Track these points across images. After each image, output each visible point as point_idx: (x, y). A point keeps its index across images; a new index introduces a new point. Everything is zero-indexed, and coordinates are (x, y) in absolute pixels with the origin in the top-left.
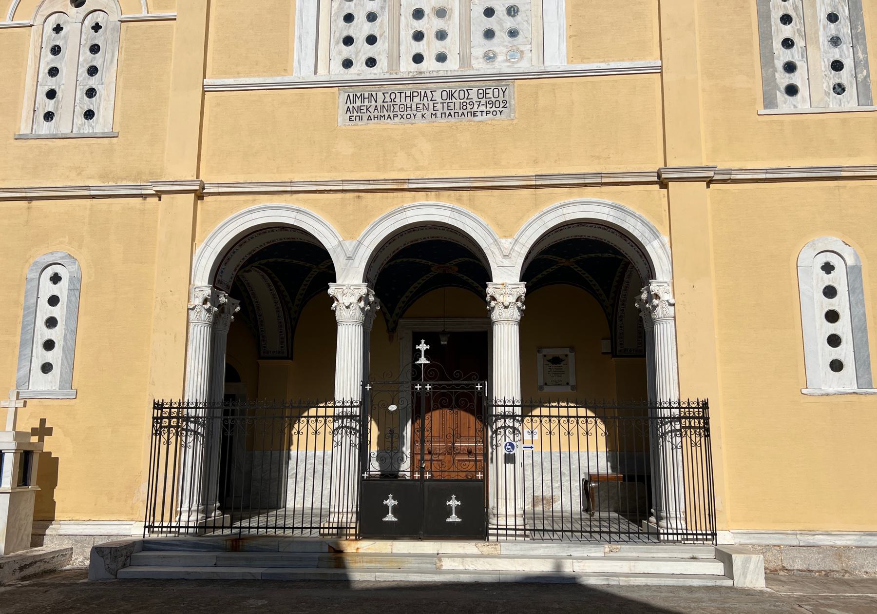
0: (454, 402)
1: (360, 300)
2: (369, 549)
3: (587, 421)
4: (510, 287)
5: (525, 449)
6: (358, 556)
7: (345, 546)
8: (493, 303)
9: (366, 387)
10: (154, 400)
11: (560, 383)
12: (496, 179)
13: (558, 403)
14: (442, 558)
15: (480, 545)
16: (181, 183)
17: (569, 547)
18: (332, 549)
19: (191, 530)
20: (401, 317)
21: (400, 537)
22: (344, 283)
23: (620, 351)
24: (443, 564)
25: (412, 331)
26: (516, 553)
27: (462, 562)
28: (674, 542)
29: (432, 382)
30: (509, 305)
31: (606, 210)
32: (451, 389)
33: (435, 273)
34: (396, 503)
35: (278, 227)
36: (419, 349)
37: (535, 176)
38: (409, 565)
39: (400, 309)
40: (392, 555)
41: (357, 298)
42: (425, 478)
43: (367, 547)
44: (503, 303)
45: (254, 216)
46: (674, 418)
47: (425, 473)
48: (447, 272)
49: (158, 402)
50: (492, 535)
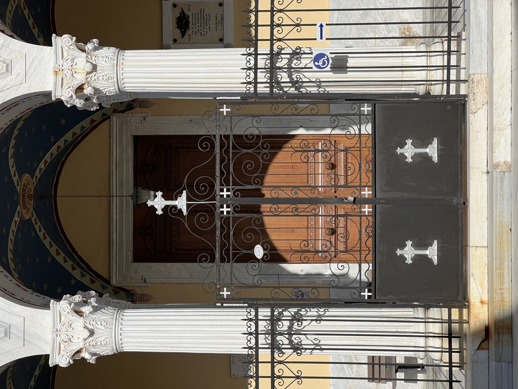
0: (250, 151)
1: (79, 313)
2: (481, 284)
3: (279, 25)
4: (60, 62)
5: (324, 37)
6: (493, 302)
7: (478, 324)
8: (88, 91)
9: (225, 297)
11: (219, 18)
13: (251, 11)
14: (494, 161)
15: (474, 107)
18: (483, 344)
20: (108, 282)
21: (462, 275)
22: (50, 341)
24: (502, 161)
26: (485, 50)
27: (500, 130)
29: (217, 187)
30: (92, 63)
33: (33, 216)
34: (409, 243)
36: (163, 210)
38: (505, 215)
39: (95, 282)
40: (490, 247)
41: (76, 317)
42: (371, 197)
43: (479, 287)
44: (85, 340)
46: (271, 78)
47: (363, 197)
48: (32, 192)
50: (458, 89)
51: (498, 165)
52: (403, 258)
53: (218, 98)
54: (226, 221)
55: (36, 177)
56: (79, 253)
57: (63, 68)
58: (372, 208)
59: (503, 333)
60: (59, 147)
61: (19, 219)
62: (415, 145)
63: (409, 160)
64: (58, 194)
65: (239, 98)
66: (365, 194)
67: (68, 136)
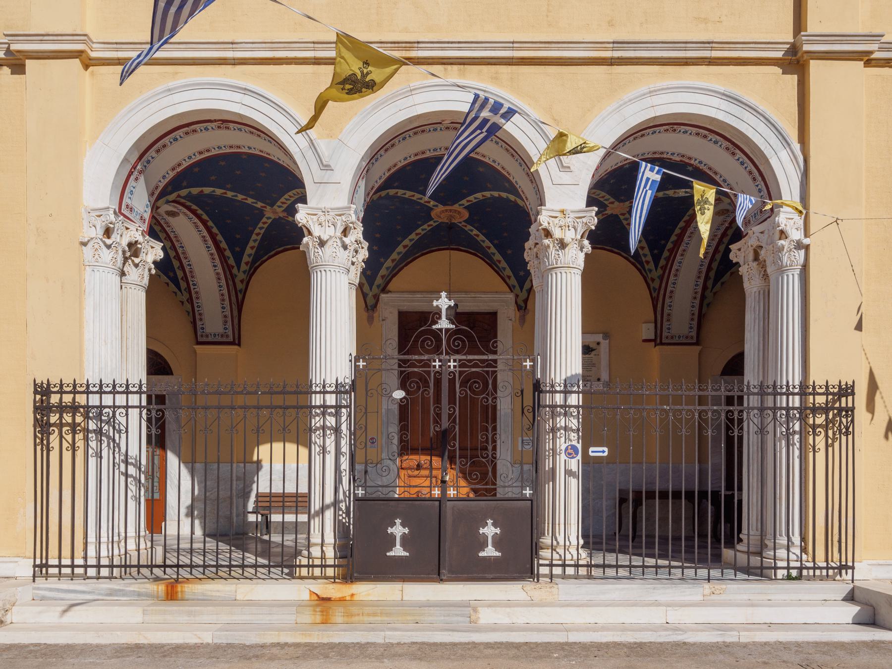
0: (490, 386)
4: (572, 215)
10: (35, 381)
12: (553, 45)
14: (479, 609)
16: (55, 38)
17: (654, 589)
20: (384, 290)
22: (320, 206)
23: (667, 337)
24: (480, 616)
25: (398, 310)
28: (821, 579)
29: (458, 357)
31: (716, 101)
32: (487, 366)
33: (435, 222)
35: (215, 121)
36: (437, 306)
37: (613, 43)
39: (383, 279)
40: (402, 603)
42: (448, 496)
45: (177, 98)
49: (42, 383)
51: (476, 612)
52: (393, 524)
53: (539, 357)
54: (427, 364)
55: (466, 226)
56: (405, 268)
57: (567, 218)
58: (453, 497)
59: (323, 615)
60: (489, 248)
61: (431, 206)
62: (495, 536)
63: (481, 531)
64: (452, 251)
65: (539, 377)
66: (450, 491)
67: (498, 257)
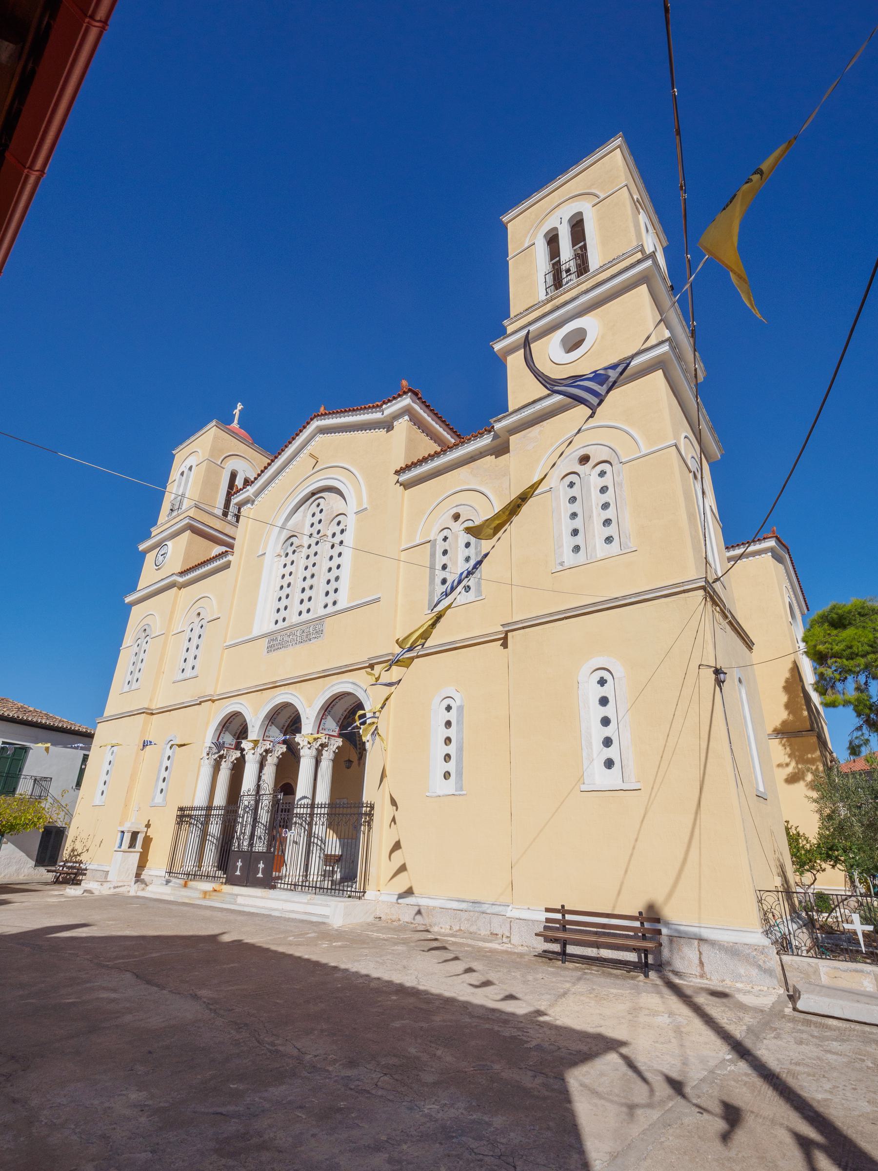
19: (280, 881)
28: (287, 889)
41: (206, 754)
